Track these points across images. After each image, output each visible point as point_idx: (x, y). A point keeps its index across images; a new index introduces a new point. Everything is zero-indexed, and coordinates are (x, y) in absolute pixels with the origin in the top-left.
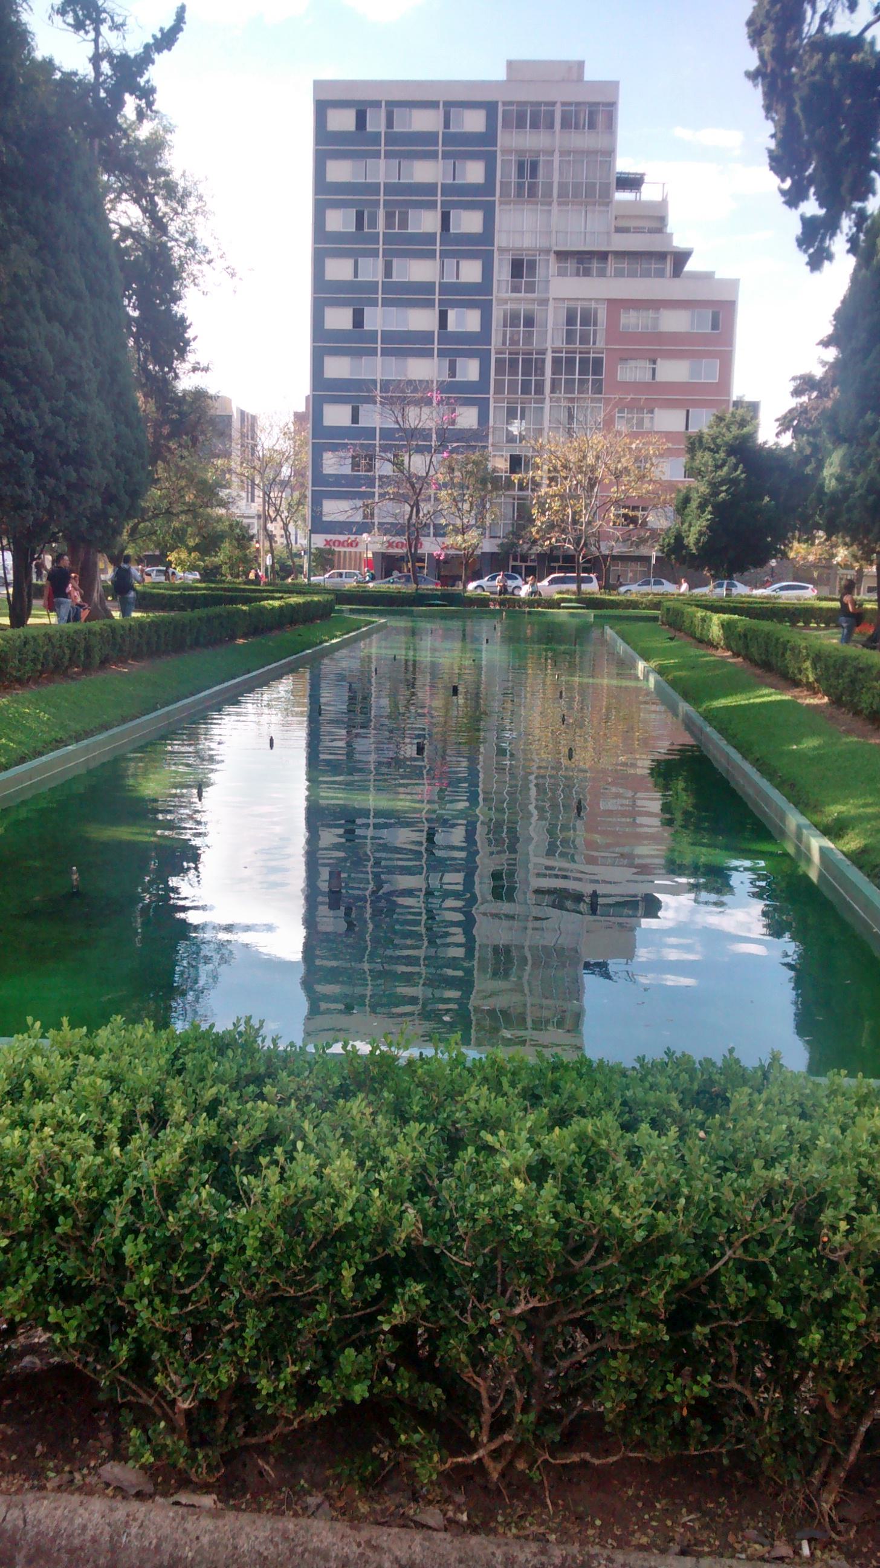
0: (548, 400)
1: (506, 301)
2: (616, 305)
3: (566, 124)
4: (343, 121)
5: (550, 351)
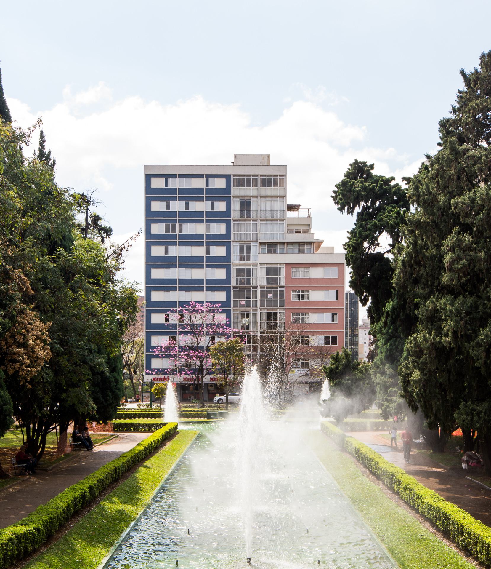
0: (259, 310)
1: (237, 265)
2: (288, 266)
3: (263, 185)
4: (157, 183)
5: (259, 287)
